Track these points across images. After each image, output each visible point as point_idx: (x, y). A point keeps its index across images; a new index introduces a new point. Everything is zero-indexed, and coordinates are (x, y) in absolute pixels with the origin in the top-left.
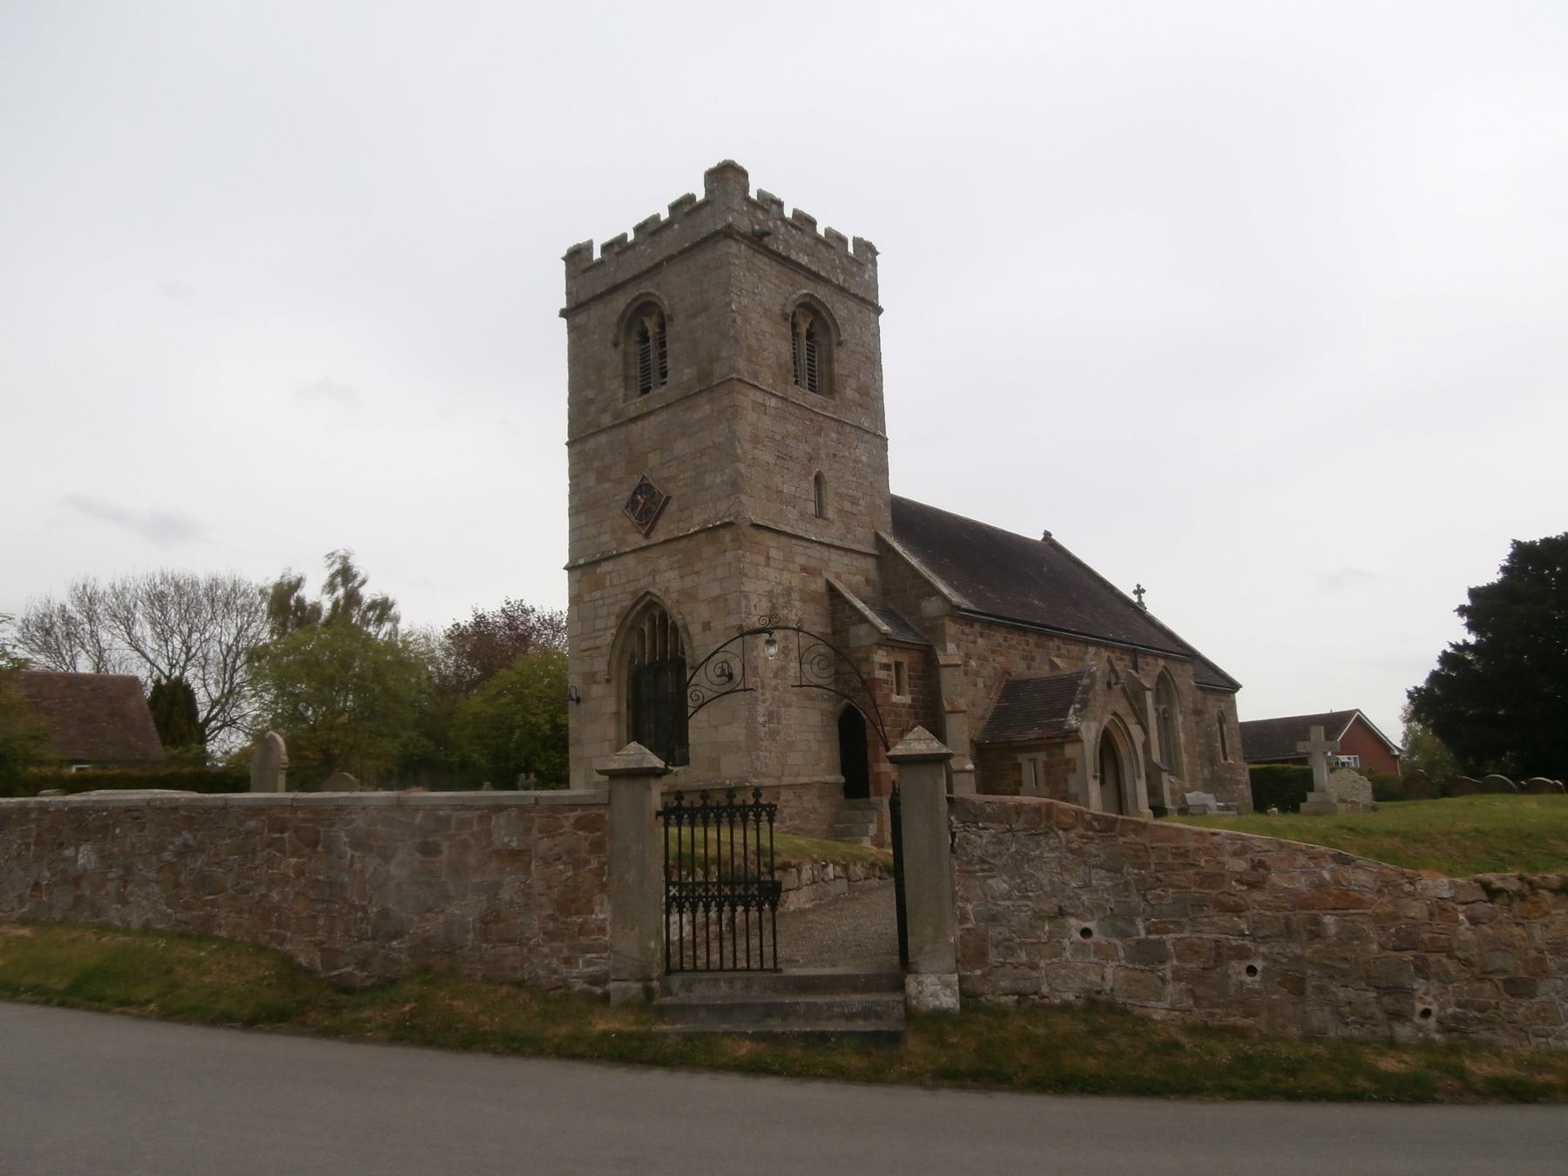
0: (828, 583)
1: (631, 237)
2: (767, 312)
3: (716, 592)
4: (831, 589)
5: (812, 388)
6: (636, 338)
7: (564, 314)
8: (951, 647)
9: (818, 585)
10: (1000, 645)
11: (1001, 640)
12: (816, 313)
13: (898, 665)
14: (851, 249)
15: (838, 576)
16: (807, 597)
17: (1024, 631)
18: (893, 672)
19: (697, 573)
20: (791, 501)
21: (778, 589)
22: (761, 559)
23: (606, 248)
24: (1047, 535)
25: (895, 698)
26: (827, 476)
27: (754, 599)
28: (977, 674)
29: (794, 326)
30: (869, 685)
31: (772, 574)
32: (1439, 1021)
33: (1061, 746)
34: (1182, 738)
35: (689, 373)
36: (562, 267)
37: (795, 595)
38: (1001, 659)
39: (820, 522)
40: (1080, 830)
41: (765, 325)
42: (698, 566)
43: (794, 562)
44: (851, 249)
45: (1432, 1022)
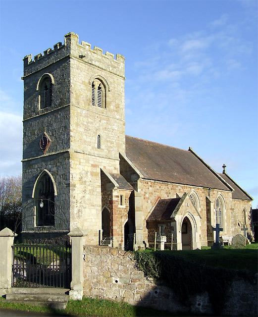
1: (43, 55)
2: (83, 83)
5: (99, 106)
10: (158, 189)
12: (101, 81)
15: (105, 167)
18: (120, 198)
20: (89, 144)
25: (120, 206)
26: (102, 135)
28: (149, 198)
31: (81, 167)
32: (202, 307)
33: (170, 223)
34: (225, 218)
37: (89, 174)
38: (158, 194)
41: (83, 87)
45: (200, 307)
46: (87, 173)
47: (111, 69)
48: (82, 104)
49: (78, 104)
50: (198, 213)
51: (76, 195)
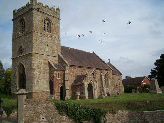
0: (49, 61)
2: (39, 21)
3: (29, 63)
4: (49, 63)
6: (21, 24)
7: (12, 20)
8: (67, 71)
9: (47, 62)
10: (76, 70)
11: (77, 69)
12: (49, 20)
13: (58, 74)
14: (55, 10)
15: (50, 60)
16: (44, 63)
17: (81, 68)
18: (58, 75)
19: (27, 60)
20: (42, 49)
21: (39, 63)
22: (37, 58)
23: (18, 10)
24: (93, 52)
25: (58, 79)
27: (35, 64)
29: (44, 22)
30: (53, 77)
31: (38, 60)
33: (82, 85)
34: (110, 83)
35: (27, 30)
36: (12, 13)
38: (77, 72)
39: (47, 52)
40: (43, 104)
41: (39, 23)
42: (27, 59)
43: (42, 58)
44: (55, 10)
47: (53, 15)
48: (39, 31)
49: (37, 31)
51: (35, 74)
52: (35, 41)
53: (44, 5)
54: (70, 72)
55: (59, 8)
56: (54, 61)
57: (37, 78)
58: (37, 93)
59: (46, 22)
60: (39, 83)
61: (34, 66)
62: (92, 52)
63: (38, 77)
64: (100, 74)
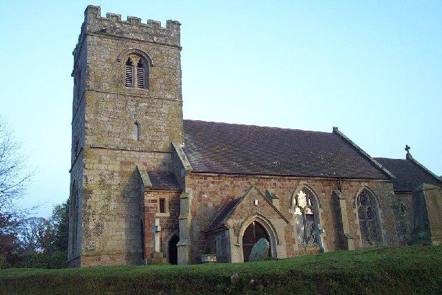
10: (227, 186)
12: (141, 56)
16: (122, 174)
18: (158, 203)
31: (103, 167)
34: (382, 221)
46: (112, 174)
47: (155, 39)
48: (106, 86)
49: (99, 87)
50: (279, 213)
51: (92, 204)
52: (92, 117)
53: (124, 19)
54: (202, 192)
55: (91, 11)
56: (149, 162)
57: (96, 217)
58: (98, 255)
59: (135, 61)
60: (102, 228)
61: (89, 182)
62: (331, 131)
63: (100, 212)
64: (334, 194)
